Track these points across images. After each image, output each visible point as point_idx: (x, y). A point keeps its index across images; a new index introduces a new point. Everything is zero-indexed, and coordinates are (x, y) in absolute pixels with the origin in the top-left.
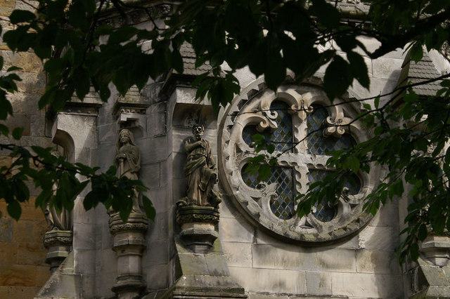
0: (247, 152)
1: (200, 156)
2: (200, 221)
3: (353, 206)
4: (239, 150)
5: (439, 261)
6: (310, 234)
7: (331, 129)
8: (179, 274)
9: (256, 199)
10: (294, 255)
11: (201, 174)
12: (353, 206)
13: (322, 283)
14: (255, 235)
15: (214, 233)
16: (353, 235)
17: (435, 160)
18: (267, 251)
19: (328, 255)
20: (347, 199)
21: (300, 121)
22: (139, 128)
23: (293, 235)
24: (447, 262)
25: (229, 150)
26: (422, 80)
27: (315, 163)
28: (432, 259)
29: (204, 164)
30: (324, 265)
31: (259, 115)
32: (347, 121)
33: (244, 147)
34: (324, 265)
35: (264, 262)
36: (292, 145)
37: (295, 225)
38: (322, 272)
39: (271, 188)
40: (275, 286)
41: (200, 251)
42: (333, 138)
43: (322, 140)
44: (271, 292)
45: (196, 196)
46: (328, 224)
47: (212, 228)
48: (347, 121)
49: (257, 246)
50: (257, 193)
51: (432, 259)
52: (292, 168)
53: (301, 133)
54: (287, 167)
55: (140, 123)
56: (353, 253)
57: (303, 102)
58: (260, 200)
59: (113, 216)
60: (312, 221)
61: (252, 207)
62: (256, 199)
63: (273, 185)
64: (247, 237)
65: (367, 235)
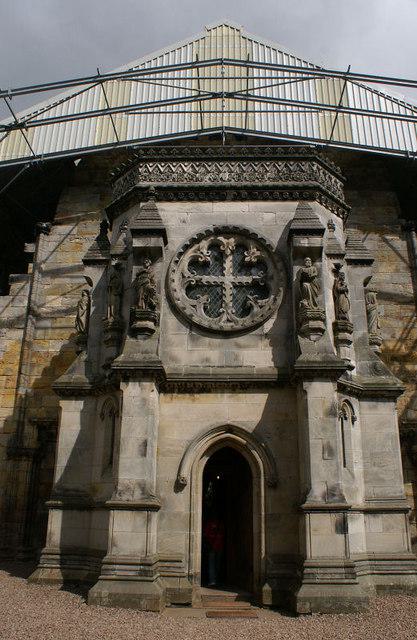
2: (141, 319)
3: (261, 307)
4: (183, 277)
5: (313, 337)
6: (228, 326)
7: (247, 259)
8: (118, 354)
9: (194, 306)
10: (217, 341)
12: (261, 307)
13: (236, 358)
14: (191, 330)
15: (323, 326)
16: (260, 324)
18: (198, 339)
19: (241, 340)
20: (256, 302)
21: (227, 256)
23: (215, 327)
25: (176, 277)
26: (383, 89)
27: (236, 281)
28: (308, 337)
30: (239, 346)
31: (198, 254)
32: (258, 253)
33: (187, 274)
35: (197, 346)
38: (236, 351)
43: (243, 267)
45: (142, 304)
48: (258, 253)
49: (191, 336)
50: (194, 302)
51: (308, 337)
52: (221, 286)
53: (228, 264)
54: (218, 286)
57: (228, 243)
59: (111, 315)
61: (188, 311)
62: (194, 306)
63: (205, 297)
64: (185, 331)
65: (268, 326)
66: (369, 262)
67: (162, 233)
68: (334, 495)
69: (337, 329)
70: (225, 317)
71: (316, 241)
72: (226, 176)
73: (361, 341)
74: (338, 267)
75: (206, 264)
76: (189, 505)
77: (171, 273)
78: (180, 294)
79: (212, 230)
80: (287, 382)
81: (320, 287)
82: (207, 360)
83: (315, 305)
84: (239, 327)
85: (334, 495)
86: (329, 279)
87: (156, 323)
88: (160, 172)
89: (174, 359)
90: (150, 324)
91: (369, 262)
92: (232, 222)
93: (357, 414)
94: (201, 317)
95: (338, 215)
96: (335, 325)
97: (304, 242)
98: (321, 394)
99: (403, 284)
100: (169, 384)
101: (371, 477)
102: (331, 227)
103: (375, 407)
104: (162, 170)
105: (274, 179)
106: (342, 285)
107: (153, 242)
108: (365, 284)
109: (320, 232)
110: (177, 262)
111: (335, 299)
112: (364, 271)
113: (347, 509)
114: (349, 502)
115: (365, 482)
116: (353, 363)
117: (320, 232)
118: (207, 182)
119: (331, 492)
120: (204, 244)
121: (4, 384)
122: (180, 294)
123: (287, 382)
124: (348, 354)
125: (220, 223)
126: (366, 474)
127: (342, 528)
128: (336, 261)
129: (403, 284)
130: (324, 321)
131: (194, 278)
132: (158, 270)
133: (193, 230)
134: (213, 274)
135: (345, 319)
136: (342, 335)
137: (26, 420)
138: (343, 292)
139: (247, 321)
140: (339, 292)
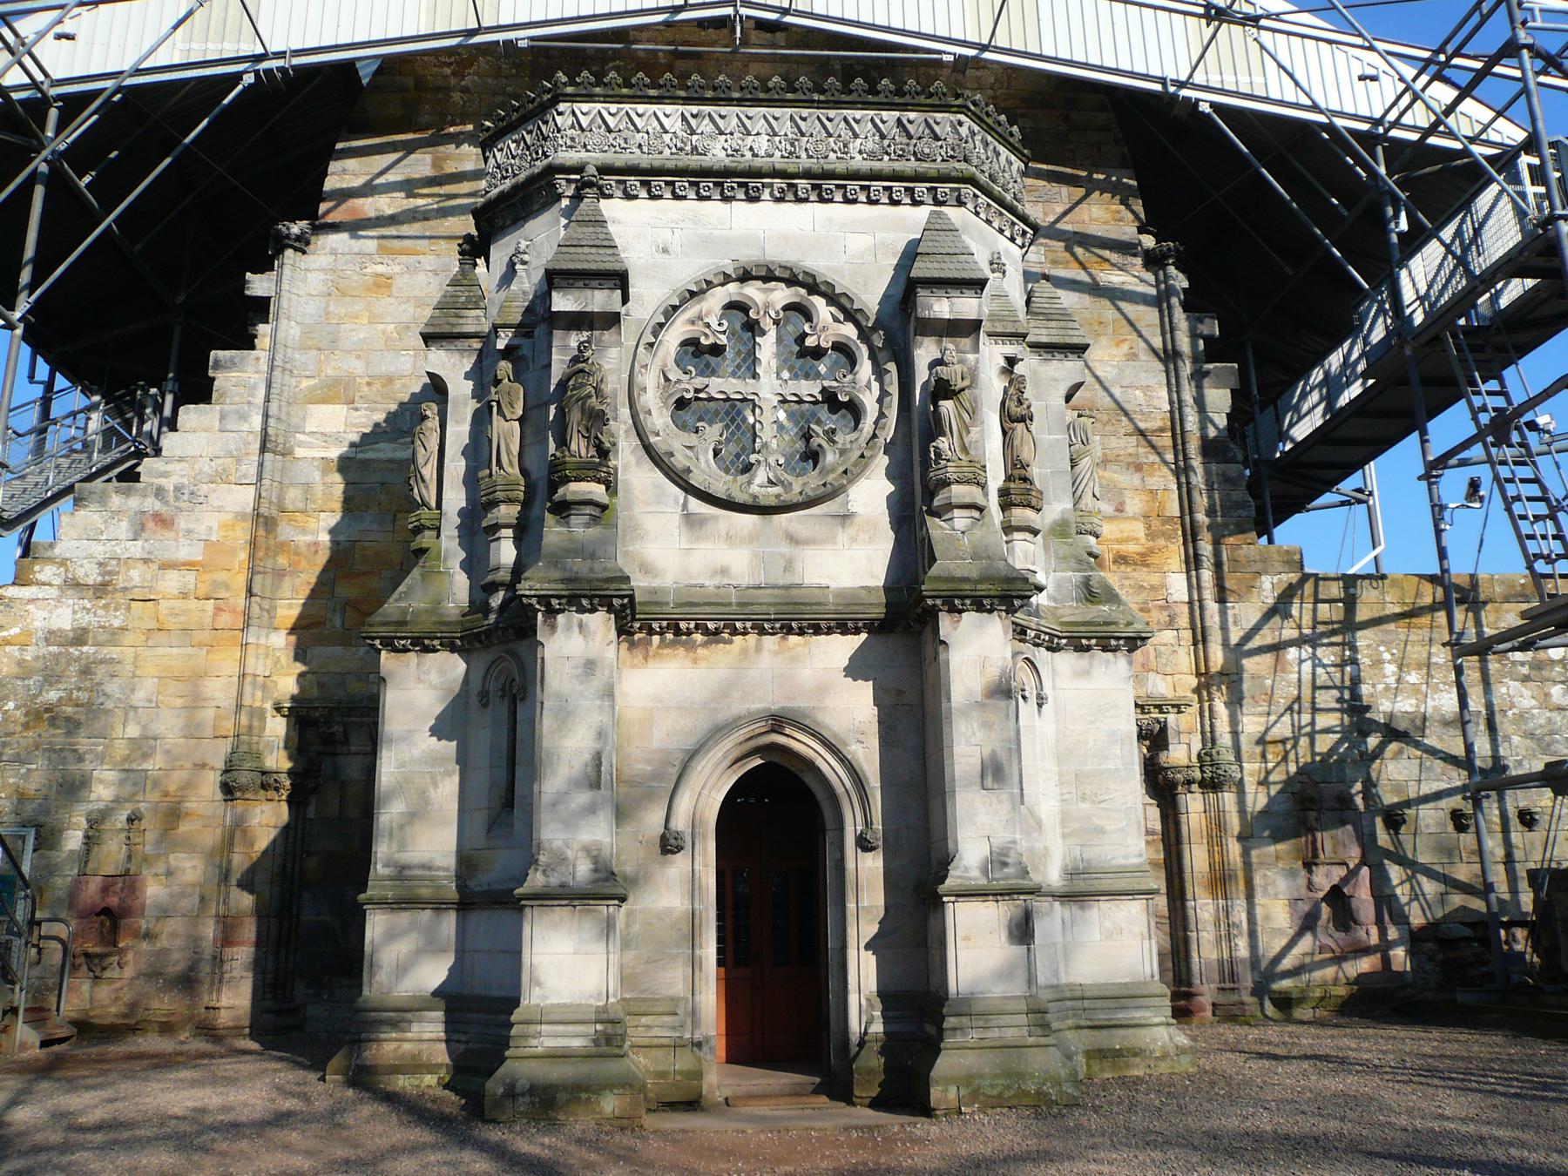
0: (679, 381)
1: (583, 385)
3: (843, 452)
4: (667, 379)
6: (769, 495)
11: (583, 410)
17: (1461, 634)
22: (523, 358)
23: (740, 497)
24: (973, 525)
25: (650, 380)
29: (589, 396)
34: (793, 539)
36: (749, 364)
37: (750, 483)
39: (713, 432)
40: (714, 574)
41: (577, 525)
42: (818, 353)
44: (707, 583)
46: (801, 480)
47: (976, 490)
50: (692, 439)
53: (767, 347)
55: (525, 351)
56: (839, 520)
57: (767, 306)
58: (699, 454)
60: (776, 476)
63: (718, 427)
66: (1080, 349)
67: (619, 280)
68: (1005, 864)
69: (1007, 501)
70: (761, 476)
71: (965, 306)
72: (762, 145)
73: (1061, 529)
74: (1011, 361)
75: (717, 350)
76: (684, 889)
77: (636, 370)
78: (659, 419)
79: (730, 271)
80: (902, 626)
81: (973, 412)
82: (724, 571)
83: (965, 449)
84: (793, 497)
85: (1005, 864)
86: (992, 387)
87: (611, 487)
88: (610, 131)
89: (646, 569)
90: (597, 491)
91: (1080, 349)
92: (778, 254)
93: (1048, 691)
94: (706, 472)
95: (1012, 240)
96: (1004, 493)
97: (941, 307)
98: (974, 648)
99: (1146, 389)
100: (636, 619)
101: (1076, 825)
102: (997, 265)
103: (1086, 673)
104: (611, 121)
105: (872, 155)
106: (1020, 402)
107: (599, 300)
108: (1068, 398)
109: (979, 285)
110: (651, 345)
111: (1004, 433)
112: (1065, 371)
113: (1035, 891)
114: (1036, 878)
115: (1064, 836)
116: (1041, 578)
117: (979, 285)
118: (717, 154)
119: (998, 860)
120: (719, 297)
121: (209, 620)
122: (659, 419)
123: (902, 626)
124: (1026, 555)
125: (749, 255)
126: (1065, 818)
127: (1023, 931)
128: (1010, 349)
129: (1146, 389)
130: (983, 486)
131: (689, 384)
132: (611, 359)
133: (687, 272)
134: (734, 374)
135: (1025, 479)
136: (1021, 515)
137: (268, 706)
138: (1022, 419)
139: (811, 481)
140: (1014, 417)
